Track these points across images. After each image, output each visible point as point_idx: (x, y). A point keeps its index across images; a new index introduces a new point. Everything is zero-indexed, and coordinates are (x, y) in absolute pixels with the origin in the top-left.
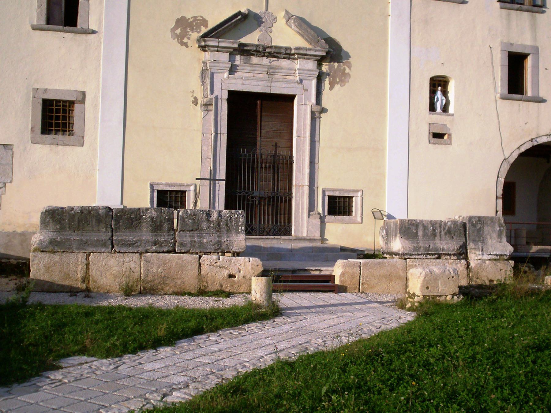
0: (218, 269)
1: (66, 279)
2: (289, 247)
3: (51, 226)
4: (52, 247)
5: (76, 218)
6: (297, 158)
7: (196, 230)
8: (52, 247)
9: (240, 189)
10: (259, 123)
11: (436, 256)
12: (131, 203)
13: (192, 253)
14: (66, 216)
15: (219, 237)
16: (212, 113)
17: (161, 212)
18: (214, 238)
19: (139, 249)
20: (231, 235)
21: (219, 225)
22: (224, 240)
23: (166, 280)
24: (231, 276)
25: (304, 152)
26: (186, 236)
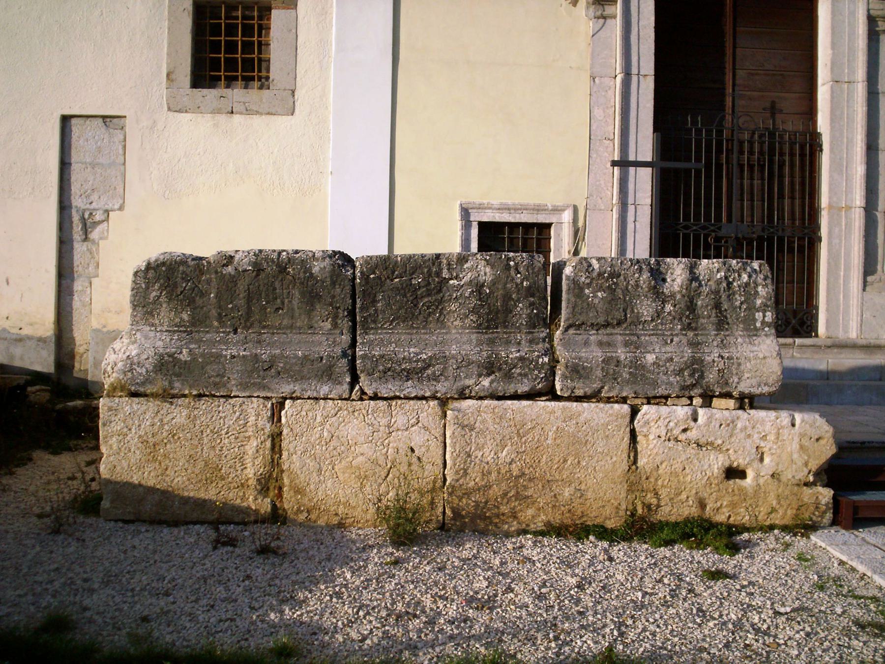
0: (692, 451)
1: (209, 481)
2: (822, 366)
3: (165, 315)
4: (168, 380)
5: (242, 286)
6: (833, 138)
7: (619, 324)
8: (168, 380)
9: (687, 217)
10: (729, 52)
12: (412, 243)
13: (608, 400)
14: (209, 282)
15: (694, 345)
16: (617, 24)
17: (508, 267)
18: (679, 350)
19: (439, 387)
20: (731, 340)
21: (691, 306)
22: (712, 354)
23: (526, 488)
24: (734, 473)
25: (851, 120)
26: (586, 343)
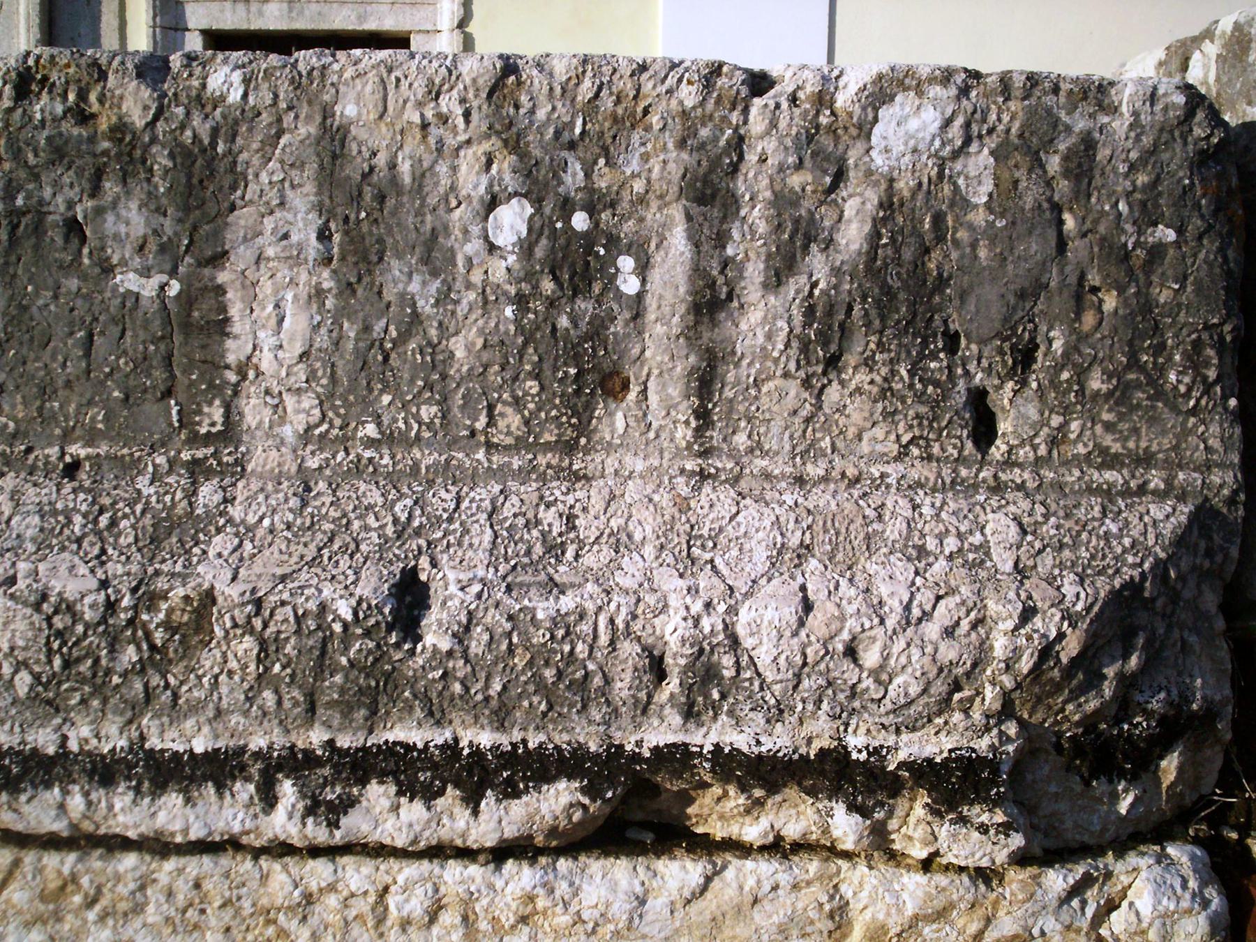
11: (557, 800)
